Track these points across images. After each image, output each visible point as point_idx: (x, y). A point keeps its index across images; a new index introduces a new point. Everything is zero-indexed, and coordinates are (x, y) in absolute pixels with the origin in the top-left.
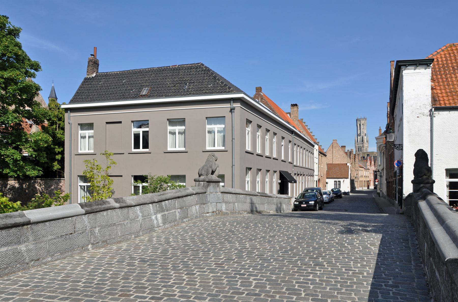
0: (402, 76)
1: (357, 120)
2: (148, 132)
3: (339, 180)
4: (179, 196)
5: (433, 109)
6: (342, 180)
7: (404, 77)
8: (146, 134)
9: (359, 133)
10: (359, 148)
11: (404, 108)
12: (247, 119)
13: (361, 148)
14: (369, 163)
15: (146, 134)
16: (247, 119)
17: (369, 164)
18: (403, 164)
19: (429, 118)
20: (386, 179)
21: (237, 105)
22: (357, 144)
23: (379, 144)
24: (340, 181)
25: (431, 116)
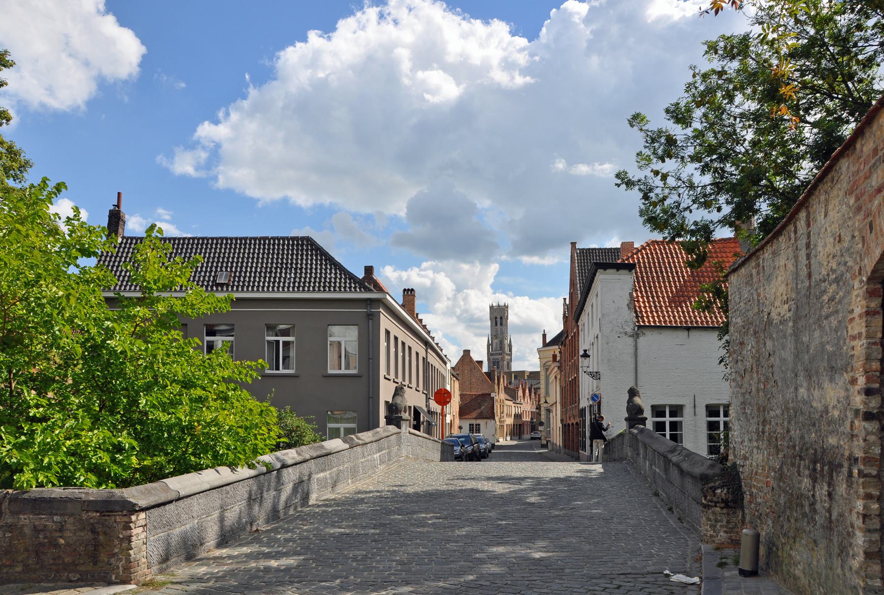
3: (478, 422)
20: (562, 421)
22: (492, 355)
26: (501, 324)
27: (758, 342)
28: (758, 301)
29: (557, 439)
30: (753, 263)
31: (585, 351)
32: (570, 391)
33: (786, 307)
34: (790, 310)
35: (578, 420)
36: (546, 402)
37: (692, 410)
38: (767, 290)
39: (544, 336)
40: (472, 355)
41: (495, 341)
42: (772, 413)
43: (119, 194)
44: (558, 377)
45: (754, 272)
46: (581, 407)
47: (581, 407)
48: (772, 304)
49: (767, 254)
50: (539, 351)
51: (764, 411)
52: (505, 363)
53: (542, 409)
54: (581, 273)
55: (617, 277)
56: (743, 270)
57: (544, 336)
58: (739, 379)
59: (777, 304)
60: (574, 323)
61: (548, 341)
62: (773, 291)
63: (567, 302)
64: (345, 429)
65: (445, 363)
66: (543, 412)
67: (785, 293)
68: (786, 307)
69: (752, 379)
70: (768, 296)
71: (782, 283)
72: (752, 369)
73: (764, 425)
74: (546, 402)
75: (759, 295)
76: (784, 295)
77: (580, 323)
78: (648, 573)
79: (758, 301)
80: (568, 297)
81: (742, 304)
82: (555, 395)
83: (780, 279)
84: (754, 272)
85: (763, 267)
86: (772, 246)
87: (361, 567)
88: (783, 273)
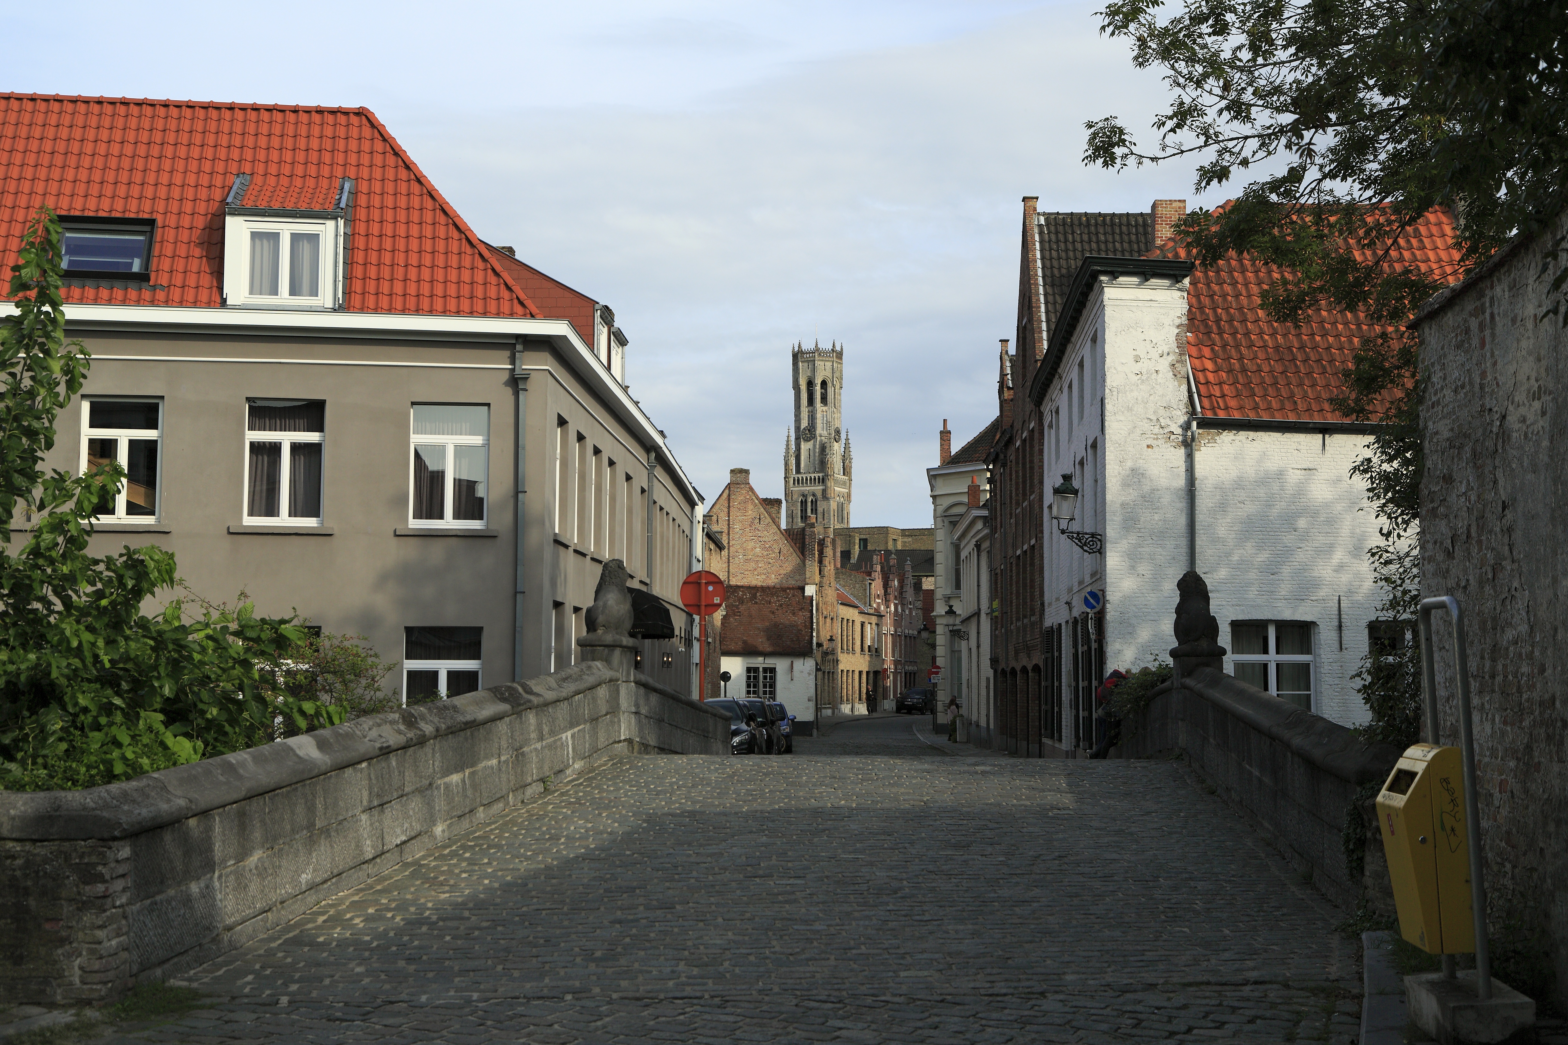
0: (1102, 307)
1: (795, 356)
2: (155, 442)
3: (770, 662)
4: (981, 649)
5: (1194, 424)
6: (781, 665)
7: (1108, 311)
8: (145, 456)
9: (804, 424)
10: (804, 503)
11: (1107, 413)
12: (559, 415)
13: (814, 503)
14: (877, 587)
15: (145, 456)
16: (559, 415)
17: (880, 592)
18: (1105, 602)
19: (1182, 452)
20: (994, 661)
21: (538, 365)
22: (797, 482)
23: (946, 502)
24: (773, 670)
25: (1189, 444)
26: (824, 400)
27: (1480, 477)
28: (1482, 387)
29: (979, 705)
30: (1470, 305)
31: (1067, 478)
32: (1018, 577)
33: (1537, 405)
34: (1544, 413)
35: (1038, 658)
36: (951, 612)
37: (1334, 635)
38: (1499, 367)
39: (945, 435)
40: (753, 480)
41: (805, 447)
42: (1510, 634)
43: (945, 421)
44: (986, 545)
45: (1474, 323)
46: (1048, 623)
47: (1048, 623)
48: (1510, 397)
49: (1500, 290)
50: (933, 476)
51: (1494, 629)
52: (833, 505)
53: (939, 630)
54: (1050, 280)
55: (1144, 293)
56: (1450, 319)
57: (945, 435)
58: (1440, 557)
59: (1521, 397)
60: (1029, 406)
61: (956, 447)
62: (1511, 369)
63: (1012, 349)
64: (451, 674)
65: (692, 505)
66: (941, 638)
67: (1534, 375)
68: (1537, 405)
69: (1469, 557)
70: (1501, 380)
71: (1530, 353)
72: (1469, 536)
73: (1494, 660)
74: (951, 612)
75: (1483, 375)
76: (1533, 381)
77: (1047, 408)
78: (1246, 983)
79: (1482, 387)
80: (1012, 335)
81: (1447, 392)
82: (976, 592)
83: (1524, 344)
84: (1474, 323)
85: (1492, 316)
86: (1509, 271)
87: (610, 971)
88: (1530, 333)
